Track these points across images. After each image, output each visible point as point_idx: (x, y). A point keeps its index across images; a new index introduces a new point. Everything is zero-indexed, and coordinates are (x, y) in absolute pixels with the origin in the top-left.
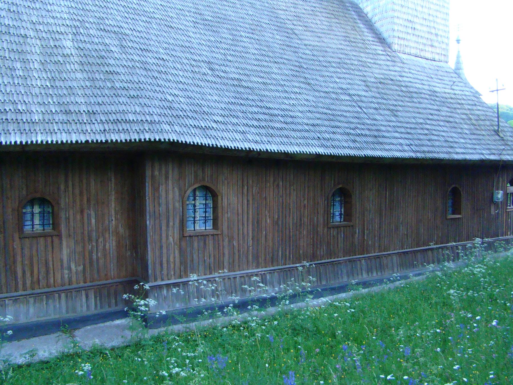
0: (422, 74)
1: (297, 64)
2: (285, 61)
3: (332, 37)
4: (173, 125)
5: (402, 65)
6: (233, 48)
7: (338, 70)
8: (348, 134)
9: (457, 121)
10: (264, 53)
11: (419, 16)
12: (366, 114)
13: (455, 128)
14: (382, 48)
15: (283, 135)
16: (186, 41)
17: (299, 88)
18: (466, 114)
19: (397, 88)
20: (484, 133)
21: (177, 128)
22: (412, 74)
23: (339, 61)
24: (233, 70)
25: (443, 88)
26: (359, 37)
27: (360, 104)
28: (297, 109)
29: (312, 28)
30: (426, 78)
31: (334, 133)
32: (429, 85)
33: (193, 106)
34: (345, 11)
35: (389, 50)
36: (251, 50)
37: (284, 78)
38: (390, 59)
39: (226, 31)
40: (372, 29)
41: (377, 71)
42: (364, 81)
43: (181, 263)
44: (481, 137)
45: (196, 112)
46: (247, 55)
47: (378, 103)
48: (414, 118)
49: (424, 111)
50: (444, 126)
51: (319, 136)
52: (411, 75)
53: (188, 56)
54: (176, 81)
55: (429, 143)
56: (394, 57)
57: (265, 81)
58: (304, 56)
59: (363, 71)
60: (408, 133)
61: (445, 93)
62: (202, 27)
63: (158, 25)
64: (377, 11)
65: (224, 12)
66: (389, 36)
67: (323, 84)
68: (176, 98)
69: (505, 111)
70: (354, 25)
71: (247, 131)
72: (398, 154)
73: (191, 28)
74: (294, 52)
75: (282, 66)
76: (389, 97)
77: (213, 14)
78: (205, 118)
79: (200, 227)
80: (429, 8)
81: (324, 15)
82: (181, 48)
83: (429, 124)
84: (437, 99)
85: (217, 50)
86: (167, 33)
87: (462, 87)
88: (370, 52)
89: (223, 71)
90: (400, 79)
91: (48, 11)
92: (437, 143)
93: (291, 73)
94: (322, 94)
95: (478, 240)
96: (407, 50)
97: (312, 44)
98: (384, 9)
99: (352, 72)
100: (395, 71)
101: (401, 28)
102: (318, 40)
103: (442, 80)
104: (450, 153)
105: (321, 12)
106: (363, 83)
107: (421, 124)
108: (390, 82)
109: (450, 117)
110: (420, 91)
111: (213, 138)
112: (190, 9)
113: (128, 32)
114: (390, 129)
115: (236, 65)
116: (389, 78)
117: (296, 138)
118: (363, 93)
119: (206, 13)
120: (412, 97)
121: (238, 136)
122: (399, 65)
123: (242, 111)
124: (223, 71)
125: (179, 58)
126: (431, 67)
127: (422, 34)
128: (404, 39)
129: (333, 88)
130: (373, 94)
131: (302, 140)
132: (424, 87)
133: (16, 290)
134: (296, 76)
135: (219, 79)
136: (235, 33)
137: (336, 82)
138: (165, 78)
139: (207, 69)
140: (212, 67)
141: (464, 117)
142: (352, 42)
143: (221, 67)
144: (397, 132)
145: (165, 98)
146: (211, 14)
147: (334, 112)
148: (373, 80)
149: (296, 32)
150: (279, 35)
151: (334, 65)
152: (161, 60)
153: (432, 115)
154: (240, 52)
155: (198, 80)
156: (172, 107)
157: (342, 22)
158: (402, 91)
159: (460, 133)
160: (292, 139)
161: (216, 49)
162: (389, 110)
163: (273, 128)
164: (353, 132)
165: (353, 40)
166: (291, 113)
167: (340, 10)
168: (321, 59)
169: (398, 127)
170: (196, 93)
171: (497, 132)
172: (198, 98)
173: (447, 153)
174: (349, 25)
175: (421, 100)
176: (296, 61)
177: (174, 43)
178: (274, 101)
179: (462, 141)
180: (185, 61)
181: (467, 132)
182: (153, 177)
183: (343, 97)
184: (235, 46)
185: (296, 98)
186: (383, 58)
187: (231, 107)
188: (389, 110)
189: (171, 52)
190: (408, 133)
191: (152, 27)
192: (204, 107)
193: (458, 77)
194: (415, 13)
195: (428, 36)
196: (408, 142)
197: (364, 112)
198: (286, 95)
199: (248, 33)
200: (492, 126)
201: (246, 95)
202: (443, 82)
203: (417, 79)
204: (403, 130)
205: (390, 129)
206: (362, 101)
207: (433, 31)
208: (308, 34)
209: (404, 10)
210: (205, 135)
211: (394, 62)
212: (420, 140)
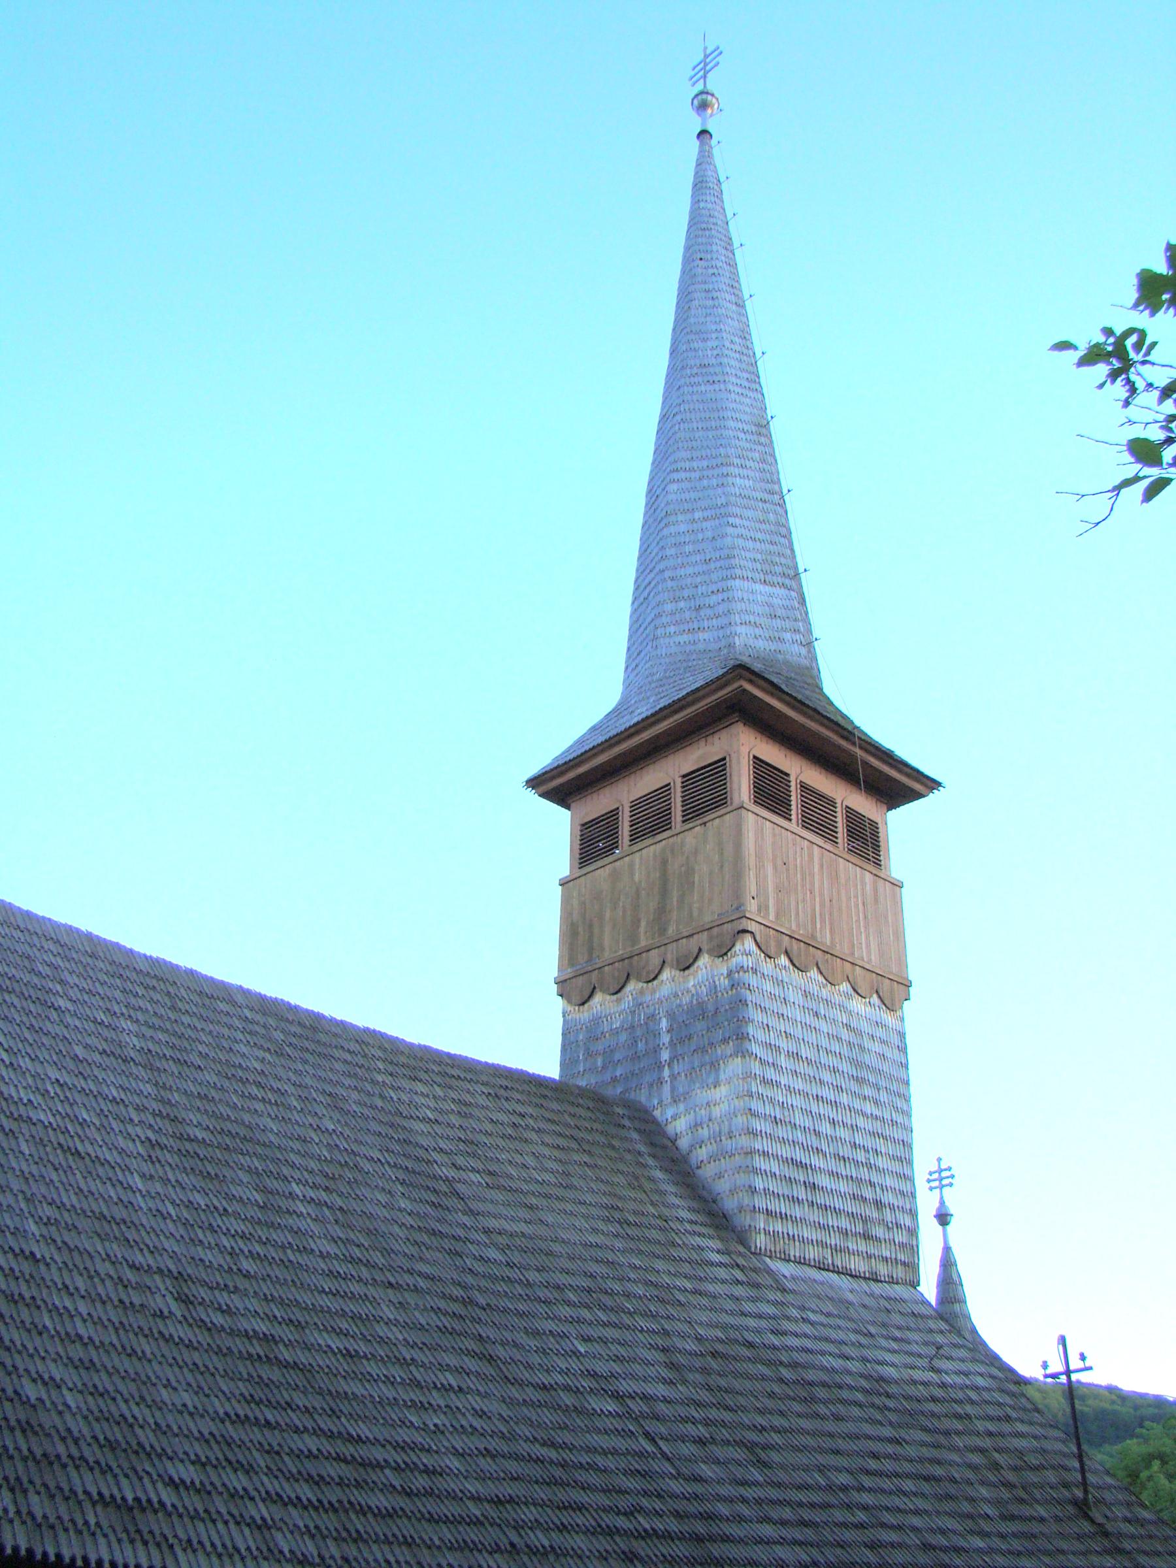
0: (840, 1322)
1: (457, 1292)
2: (422, 1283)
3: (569, 1207)
4: (25, 1491)
5: (779, 1296)
6: (263, 1233)
7: (585, 1314)
8: (611, 1532)
9: (956, 1475)
10: (357, 1252)
11: (825, 1147)
12: (668, 1459)
14: (715, 1244)
15: (394, 1535)
16: (115, 1200)
18: (982, 1451)
20: (1042, 1511)
21: (38, 1504)
22: (812, 1324)
23: (585, 1283)
24: (254, 1304)
25: (906, 1366)
26: (652, 1210)
27: (652, 1426)
28: (446, 1444)
29: (511, 1177)
30: (853, 1337)
31: (563, 1528)
32: (865, 1360)
33: (105, 1425)
34: (613, 1130)
35: (742, 1249)
36: (318, 1241)
37: (413, 1337)
38: (744, 1279)
39: (245, 1178)
40: (688, 1186)
41: (704, 1317)
42: (664, 1350)
44: (1036, 1528)
45: (112, 1446)
46: (303, 1259)
47: (707, 1423)
48: (821, 1469)
49: (853, 1446)
51: (516, 1539)
52: (807, 1329)
53: (116, 1249)
54: (63, 1333)
56: (755, 1270)
57: (352, 1345)
58: (479, 1267)
59: (662, 1317)
60: (804, 1523)
61: (914, 1382)
62: (174, 1159)
63: (36, 1143)
64: (704, 1132)
65: (247, 1118)
66: (741, 1209)
67: (536, 1359)
68: (54, 1393)
69: (1107, 1406)
70: (638, 1171)
71: (277, 1517)
73: (139, 1159)
74: (450, 1252)
75: (411, 1298)
76: (741, 1400)
77: (213, 1120)
78: (139, 1469)
80: (854, 1128)
81: (548, 1139)
82: (96, 1222)
83: (870, 1490)
84: (891, 1404)
85: (210, 1238)
86: (61, 1172)
87: (962, 1360)
88: (683, 1255)
89: (220, 1309)
90: (775, 1340)
93: (434, 1320)
94: (532, 1394)
96: (795, 1251)
97: (508, 1227)
98: (725, 1129)
99: (627, 1320)
100: (760, 1316)
101: (773, 1186)
102: (528, 1217)
103: (902, 1340)
105: (539, 1131)
106: (662, 1354)
107: (844, 1488)
108: (746, 1352)
111: (158, 1545)
112: (145, 1100)
114: (745, 1511)
115: (265, 1288)
116: (740, 1339)
117: (439, 1548)
118: (661, 1390)
119: (192, 1117)
120: (814, 1399)
122: (771, 1296)
123: (267, 1447)
124: (220, 1309)
125: (85, 1256)
126: (867, 1301)
127: (838, 1203)
128: (783, 1217)
129: (566, 1372)
131: (458, 1554)
132: (849, 1365)
134: (453, 1332)
135: (206, 1333)
137: (576, 1353)
138: (28, 1321)
139: (169, 1298)
140: (186, 1291)
141: (975, 1458)
142: (629, 1224)
143: (216, 1292)
144: (767, 1519)
145: (16, 1392)
146: (206, 1121)
147: (567, 1455)
148: (691, 1346)
149: (460, 1188)
150: (409, 1198)
151: (572, 1296)
152: (26, 1258)
153: (875, 1456)
154: (283, 1247)
155: (136, 1335)
156: (34, 1423)
158: (781, 1380)
159: (970, 1516)
160: (425, 1551)
161: (208, 1233)
162: (740, 1443)
163: (362, 1511)
164: (628, 1523)
166: (426, 1459)
167: (596, 1126)
168: (532, 1276)
169: (772, 1502)
170: (123, 1378)
171: (1082, 1508)
172: (127, 1396)
174: (622, 1173)
175: (841, 1409)
176: (454, 1282)
177: (78, 1206)
178: (375, 1412)
179: (979, 1543)
180: (105, 1268)
183: (595, 1403)
184: (269, 1227)
185: (447, 1406)
186: (722, 1273)
187: (231, 1430)
188: (740, 1443)
189: (65, 1232)
190: (804, 1523)
191: (15, 1148)
192: (141, 1427)
193: (950, 1332)
195: (850, 1207)
197: (664, 1454)
198: (415, 1395)
199: (315, 1186)
200: (1066, 1485)
201: (284, 1392)
203: (827, 1339)
204: (787, 1513)
207: (868, 1193)
208: (499, 1196)
209: (781, 1132)
210: (132, 1529)
211: (757, 1286)
212: (841, 1545)
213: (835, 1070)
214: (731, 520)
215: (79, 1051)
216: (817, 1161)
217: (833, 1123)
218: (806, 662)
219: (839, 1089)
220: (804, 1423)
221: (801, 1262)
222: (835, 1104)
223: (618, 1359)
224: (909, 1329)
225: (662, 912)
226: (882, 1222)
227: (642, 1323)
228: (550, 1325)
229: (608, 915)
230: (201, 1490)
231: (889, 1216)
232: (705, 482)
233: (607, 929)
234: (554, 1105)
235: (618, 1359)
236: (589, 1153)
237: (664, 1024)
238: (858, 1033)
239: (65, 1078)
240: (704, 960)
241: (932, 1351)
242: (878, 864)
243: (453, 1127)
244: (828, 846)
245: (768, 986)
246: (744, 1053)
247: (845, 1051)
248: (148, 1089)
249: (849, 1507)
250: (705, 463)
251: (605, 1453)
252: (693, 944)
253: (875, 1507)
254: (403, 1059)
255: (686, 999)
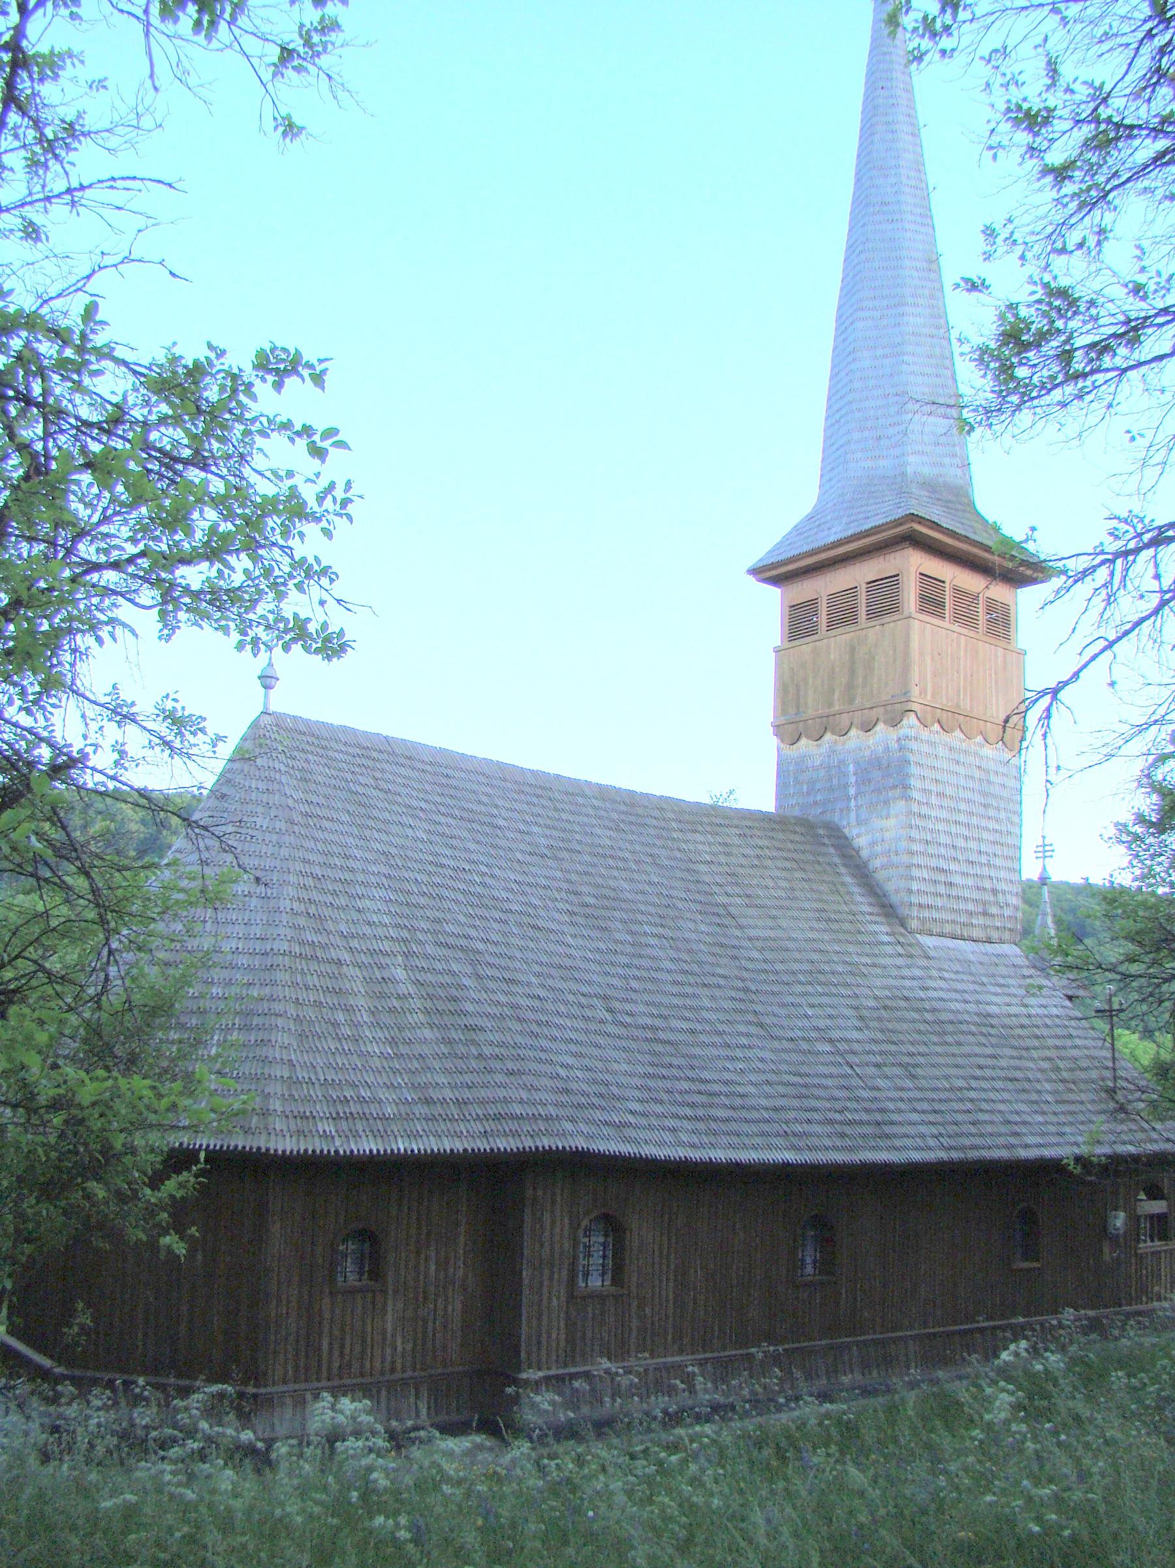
0: (965, 977)
3: (796, 914)
8: (831, 1122)
11: (960, 857)
13: (1024, 1091)
17: (747, 1035)
18: (1049, 1059)
19: (916, 1016)
27: (852, 1058)
30: (971, 987)
31: (809, 1121)
32: (979, 1002)
35: (902, 930)
37: (721, 1016)
42: (856, 1008)
43: (567, 1341)
45: (601, 1096)
46: (659, 975)
48: (947, 1077)
50: (1003, 1090)
52: (942, 984)
55: (973, 1130)
58: (749, 965)
61: (1010, 1016)
64: (878, 849)
65: (611, 883)
66: (902, 903)
72: (916, 1156)
75: (717, 992)
76: (901, 1037)
79: (595, 1282)
81: (779, 864)
84: (993, 1031)
90: (922, 994)
91: (359, 911)
92: (989, 1128)
94: (786, 1045)
95: (1069, 1314)
103: (1004, 985)
104: (1013, 1146)
107: (960, 1089)
108: (903, 1004)
109: (1016, 1068)
110: (960, 1017)
113: (480, 946)
114: (901, 1105)
115: (646, 997)
118: (855, 1035)
121: (668, 1137)
127: (967, 894)
130: (872, 1035)
132: (969, 1007)
133: (318, 1379)
134: (741, 1011)
136: (635, 928)
137: (807, 1016)
141: (1045, 1065)
147: (808, 1080)
148: (871, 1003)
149: (733, 910)
151: (801, 978)
153: (980, 1067)
157: (812, 876)
159: (1036, 1102)
162: (900, 1065)
165: (833, 916)
168: (779, 967)
173: (1005, 1147)
175: (961, 1038)
179: (1040, 1118)
180: (571, 998)
181: (1050, 1098)
182: (535, 1199)
186: (889, 949)
188: (900, 1065)
194: (951, 853)
196: (934, 1130)
202: (1007, 990)
205: (901, 1105)
206: (853, 1053)
207: (987, 885)
209: (931, 849)
211: (911, 956)
213: (969, 801)
214: (906, 358)
215: (519, 856)
216: (953, 866)
217: (966, 838)
218: (959, 482)
219: (971, 813)
220: (939, 1049)
221: (941, 935)
222: (968, 825)
223: (830, 1016)
224: (1009, 977)
225: (850, 686)
226: (997, 903)
227: (843, 991)
228: (790, 999)
229: (810, 681)
230: (644, 1115)
231: (1001, 898)
232: (884, 322)
233: (810, 692)
234: (781, 836)
235: (830, 1016)
236: (804, 870)
237: (851, 768)
238: (987, 771)
239: (520, 878)
240: (880, 727)
241: (1022, 992)
242: (1007, 638)
243: (720, 864)
244: (972, 634)
245: (925, 748)
246: (908, 799)
247: (977, 786)
248: (559, 874)
249: (961, 1100)
250: (885, 303)
251: (826, 1076)
252: (874, 714)
253: (978, 1100)
254: (687, 817)
255: (867, 753)
